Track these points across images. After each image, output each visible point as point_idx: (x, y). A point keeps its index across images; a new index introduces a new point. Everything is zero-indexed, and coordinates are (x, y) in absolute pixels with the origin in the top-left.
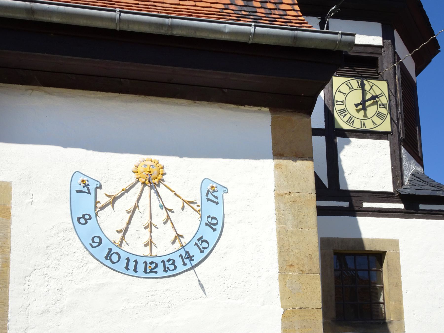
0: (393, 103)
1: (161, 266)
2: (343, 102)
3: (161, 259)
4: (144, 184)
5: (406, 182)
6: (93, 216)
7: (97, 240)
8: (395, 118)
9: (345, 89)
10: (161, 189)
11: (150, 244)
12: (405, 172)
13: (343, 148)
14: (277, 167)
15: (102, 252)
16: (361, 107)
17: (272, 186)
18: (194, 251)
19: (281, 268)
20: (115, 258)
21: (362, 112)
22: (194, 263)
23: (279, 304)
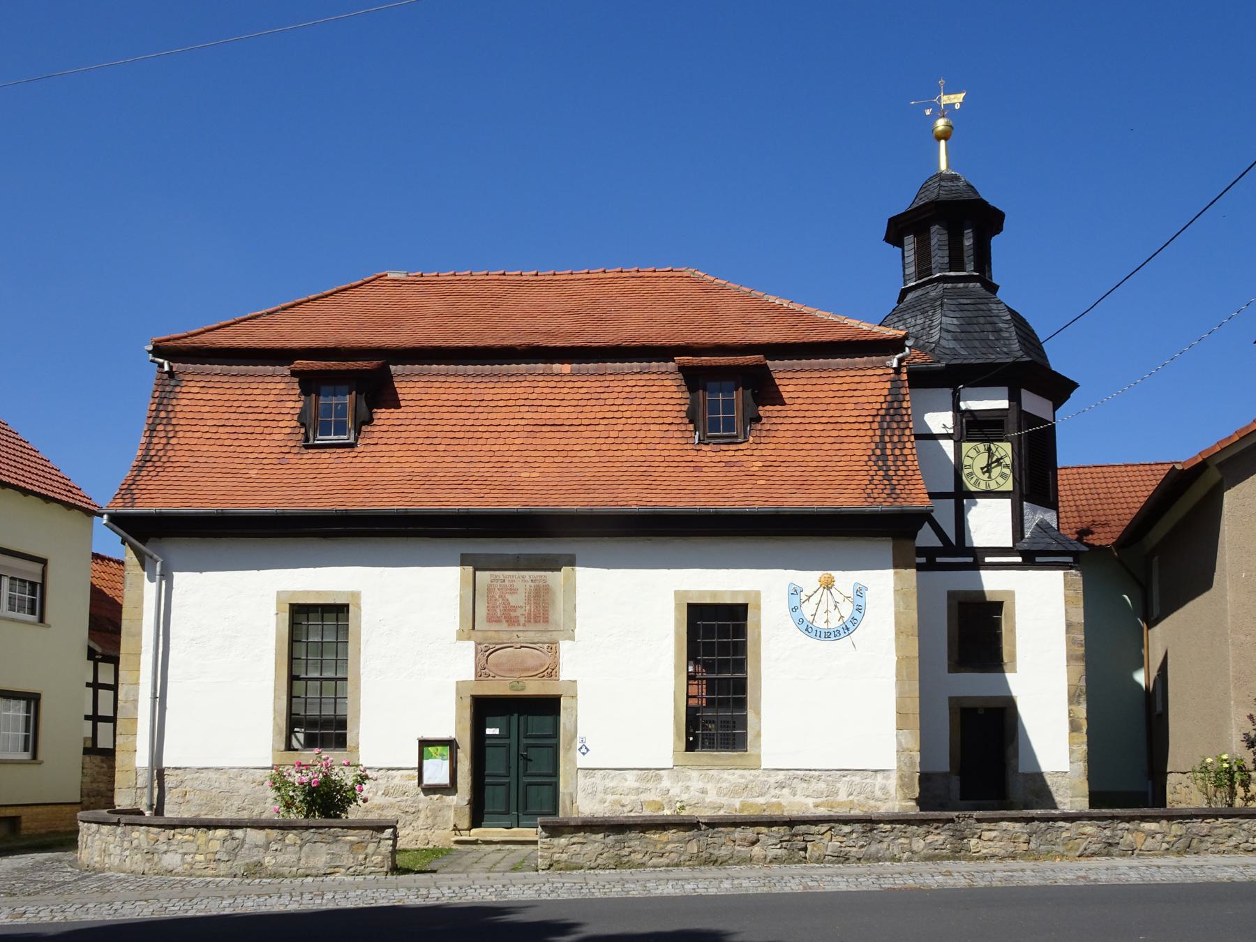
0: (1016, 463)
1: (833, 634)
2: (970, 466)
3: (833, 630)
4: (824, 588)
5: (1027, 535)
6: (799, 607)
7: (801, 620)
8: (1017, 476)
9: (973, 453)
10: (833, 590)
11: (827, 621)
12: (1026, 525)
13: (970, 509)
14: (895, 573)
15: (803, 627)
16: (986, 469)
17: (892, 586)
18: (850, 625)
19: (896, 634)
20: (810, 630)
21: (987, 474)
22: (850, 632)
23: (895, 654)
